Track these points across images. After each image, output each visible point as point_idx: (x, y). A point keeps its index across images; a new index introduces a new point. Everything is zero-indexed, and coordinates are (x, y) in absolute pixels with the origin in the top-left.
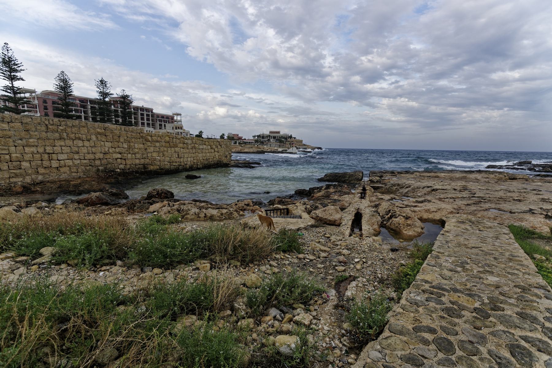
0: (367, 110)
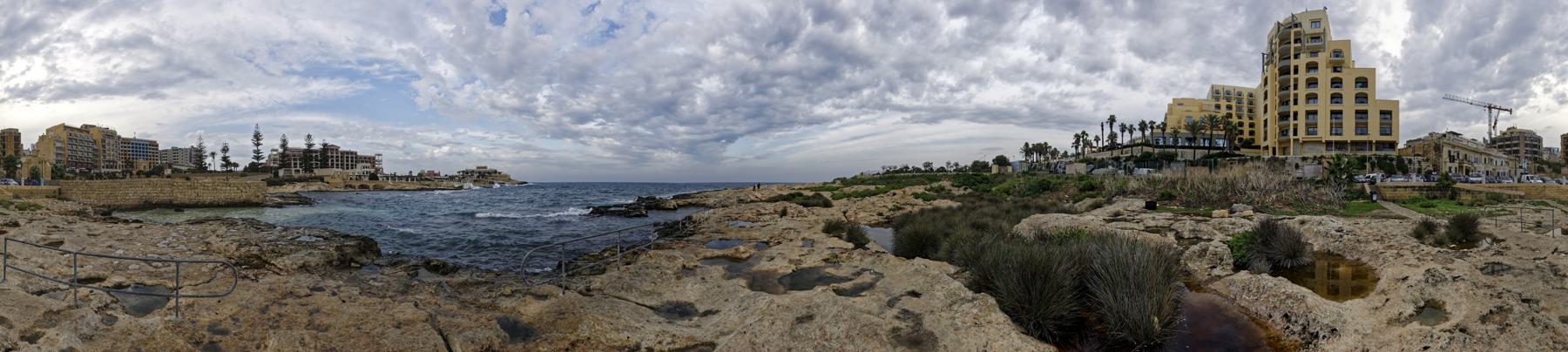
0: (580, 146)
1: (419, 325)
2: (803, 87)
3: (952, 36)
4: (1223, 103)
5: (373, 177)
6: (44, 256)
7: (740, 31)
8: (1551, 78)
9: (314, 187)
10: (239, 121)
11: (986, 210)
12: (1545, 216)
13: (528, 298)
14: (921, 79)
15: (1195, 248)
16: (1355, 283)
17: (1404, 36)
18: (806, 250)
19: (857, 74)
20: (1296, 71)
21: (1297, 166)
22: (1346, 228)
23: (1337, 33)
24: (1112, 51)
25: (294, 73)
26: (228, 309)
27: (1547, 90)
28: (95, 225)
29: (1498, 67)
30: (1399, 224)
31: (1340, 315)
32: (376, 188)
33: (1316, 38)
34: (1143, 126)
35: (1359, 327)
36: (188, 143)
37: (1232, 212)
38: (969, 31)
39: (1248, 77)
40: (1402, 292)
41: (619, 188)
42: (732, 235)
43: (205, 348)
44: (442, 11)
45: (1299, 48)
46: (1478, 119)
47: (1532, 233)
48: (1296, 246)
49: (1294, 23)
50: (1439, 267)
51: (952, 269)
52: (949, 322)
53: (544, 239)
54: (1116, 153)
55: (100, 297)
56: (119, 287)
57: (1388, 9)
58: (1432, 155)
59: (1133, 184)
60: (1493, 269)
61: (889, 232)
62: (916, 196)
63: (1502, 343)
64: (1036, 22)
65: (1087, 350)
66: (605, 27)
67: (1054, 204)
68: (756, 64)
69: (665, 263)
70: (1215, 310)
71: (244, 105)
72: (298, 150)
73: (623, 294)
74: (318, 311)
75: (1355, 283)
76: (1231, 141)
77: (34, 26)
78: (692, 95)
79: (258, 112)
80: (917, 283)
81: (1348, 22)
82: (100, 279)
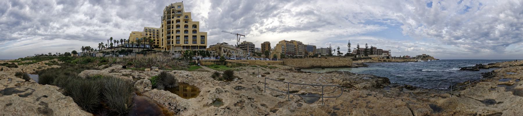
0: (457, 47)
1: (403, 107)
2: (8, 28)
3: (58, 11)
4: (148, 33)
5: (388, 58)
6: (278, 84)
7: (510, 9)
8: (258, 25)
9: (368, 61)
10: (343, 39)
11: (69, 68)
12: (256, 71)
13: (440, 98)
14: (48, 25)
15: (139, 81)
16: (192, 93)
17: (209, 11)
18: (9, 82)
19: (26, 23)
20: (173, 23)
21: (173, 54)
22: (189, 74)
23: (186, 10)
24: (111, 16)
25: (361, 23)
26: (339, 102)
27: (257, 29)
28: (295, 74)
29: (240, 21)
30: (207, 73)
31: (187, 103)
32: (389, 61)
33: (179, 11)
34: (122, 41)
35: (194, 107)
36: (326, 46)
37: (151, 69)
38: (64, 9)
39: (157, 25)
40: (208, 96)
41: (470, 61)
42: (508, 77)
43: (332, 115)
44: (411, 3)
45: (173, 15)
46: (233, 38)
47: (251, 76)
48: (173, 80)
49: (172, 7)
50: (220, 88)
51: (58, 88)
52: (57, 106)
53: (445, 78)
54: (113, 50)
55: (297, 97)
56: (303, 94)
57: (203, 3)
58: (218, 50)
59: (118, 60)
60: (238, 88)
61: (37, 76)
62: (46, 64)
63: (241, 113)
64: (86, 6)
65: (103, 115)
66: (465, 8)
67: (92, 67)
68: (515, 20)
69: (485, 86)
70: (146, 101)
71: (345, 34)
72: (363, 49)
73: (471, 96)
74: (369, 102)
75: (192, 93)
76: (151, 46)
77: (275, 8)
78: (494, 31)
79: (350, 36)
80: (46, 93)
81: (190, 6)
82: (297, 92)
